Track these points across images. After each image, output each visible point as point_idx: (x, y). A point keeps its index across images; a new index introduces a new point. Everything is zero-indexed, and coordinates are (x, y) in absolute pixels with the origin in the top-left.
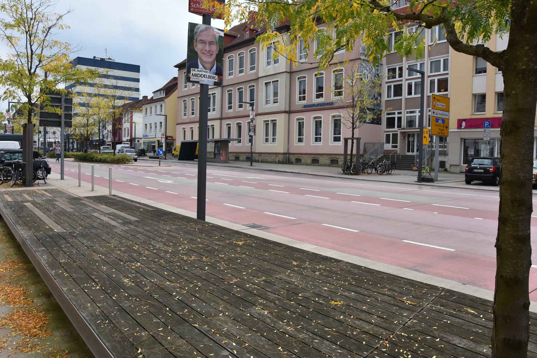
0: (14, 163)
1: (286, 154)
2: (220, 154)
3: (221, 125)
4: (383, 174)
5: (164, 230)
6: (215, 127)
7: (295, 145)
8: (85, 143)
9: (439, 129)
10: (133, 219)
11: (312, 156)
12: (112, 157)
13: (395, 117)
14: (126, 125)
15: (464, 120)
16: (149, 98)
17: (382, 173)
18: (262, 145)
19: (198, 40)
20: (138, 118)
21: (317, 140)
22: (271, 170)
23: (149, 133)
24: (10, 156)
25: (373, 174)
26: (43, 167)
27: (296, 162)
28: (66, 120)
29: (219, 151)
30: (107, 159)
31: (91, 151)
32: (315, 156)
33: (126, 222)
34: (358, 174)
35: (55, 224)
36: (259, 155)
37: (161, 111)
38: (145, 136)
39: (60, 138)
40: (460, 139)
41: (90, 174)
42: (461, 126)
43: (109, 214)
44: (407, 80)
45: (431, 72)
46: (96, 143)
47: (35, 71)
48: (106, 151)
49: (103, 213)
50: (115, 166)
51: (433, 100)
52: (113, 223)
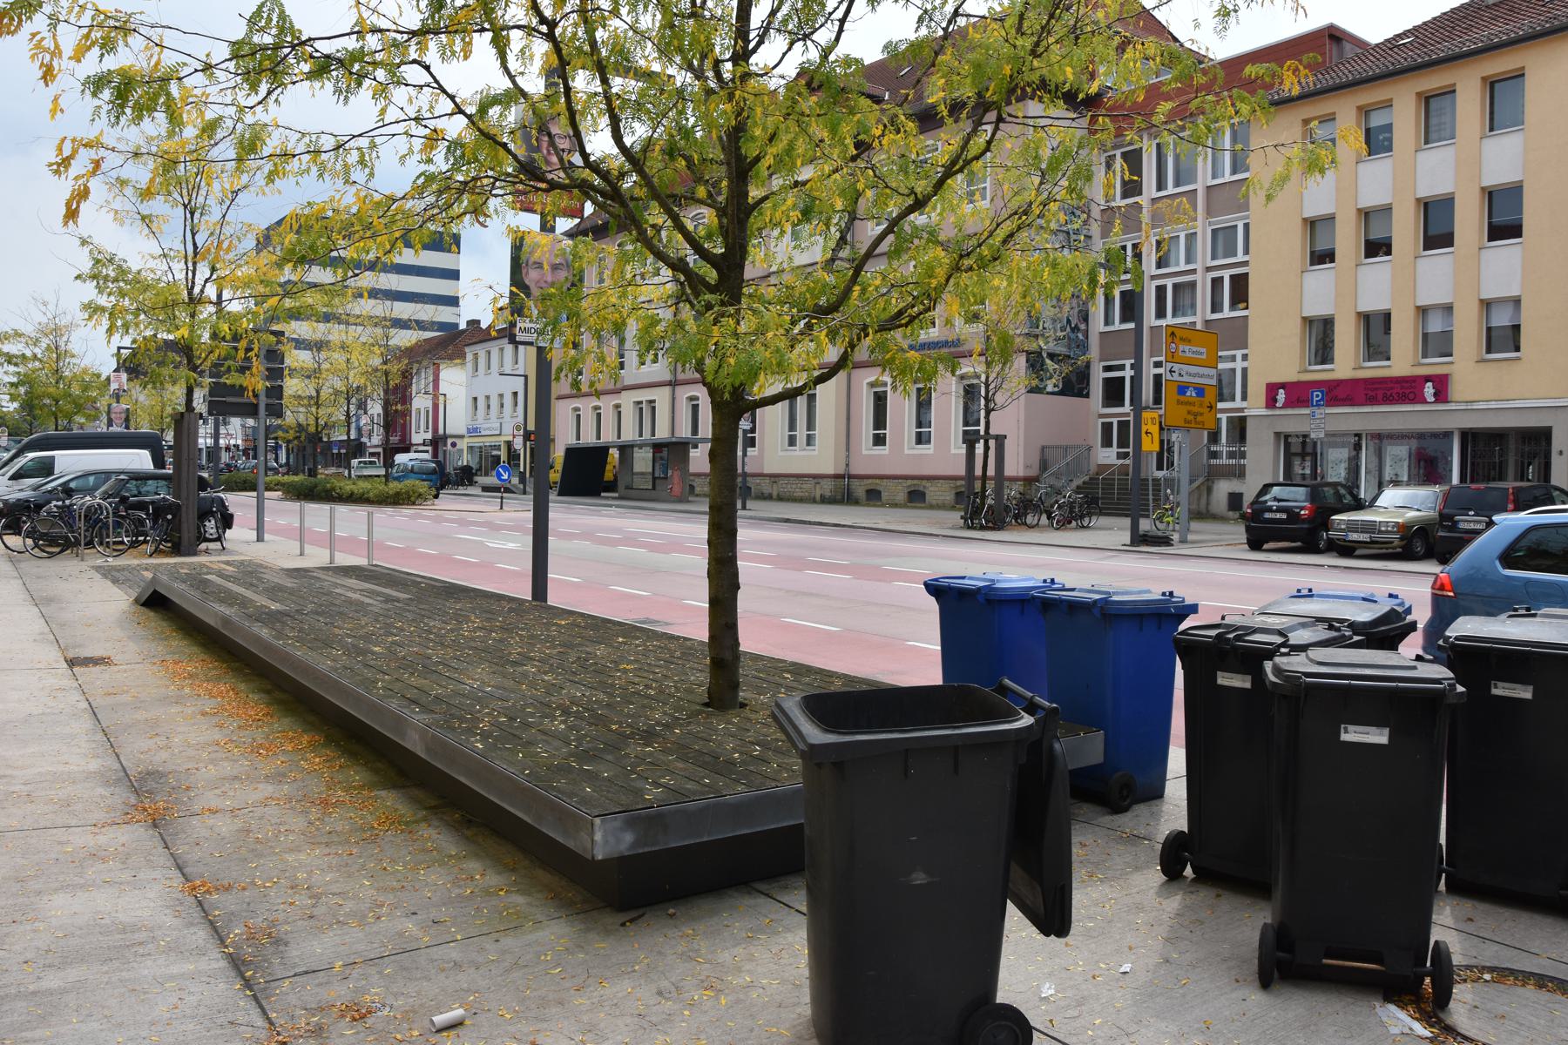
0: (153, 502)
1: (841, 477)
2: (666, 478)
3: (673, 399)
4: (1066, 529)
5: (451, 609)
6: (656, 404)
7: (864, 452)
8: (309, 450)
9: (1189, 412)
10: (402, 596)
11: (909, 482)
12: (382, 487)
13: (1124, 378)
14: (420, 403)
15: (1283, 386)
16: (484, 325)
17: (1064, 524)
18: (781, 454)
19: (530, 263)
20: (454, 380)
21: (921, 439)
22: (787, 521)
23: (483, 421)
24: (137, 487)
25: (1044, 526)
26: (218, 510)
27: (868, 499)
28: (270, 401)
29: (665, 469)
30: (368, 492)
31: (326, 472)
32: (915, 482)
33: (389, 599)
34: (1000, 529)
35: (270, 601)
36: (773, 479)
37: (516, 363)
38: (473, 431)
39: (240, 436)
40: (1272, 435)
41: (326, 530)
42: (1276, 401)
43: (361, 590)
44: (1209, 269)
45: (1214, 257)
46: (339, 450)
47: (202, 291)
48: (366, 472)
49: (355, 591)
50: (389, 510)
51: (1170, 340)
52: (368, 601)
